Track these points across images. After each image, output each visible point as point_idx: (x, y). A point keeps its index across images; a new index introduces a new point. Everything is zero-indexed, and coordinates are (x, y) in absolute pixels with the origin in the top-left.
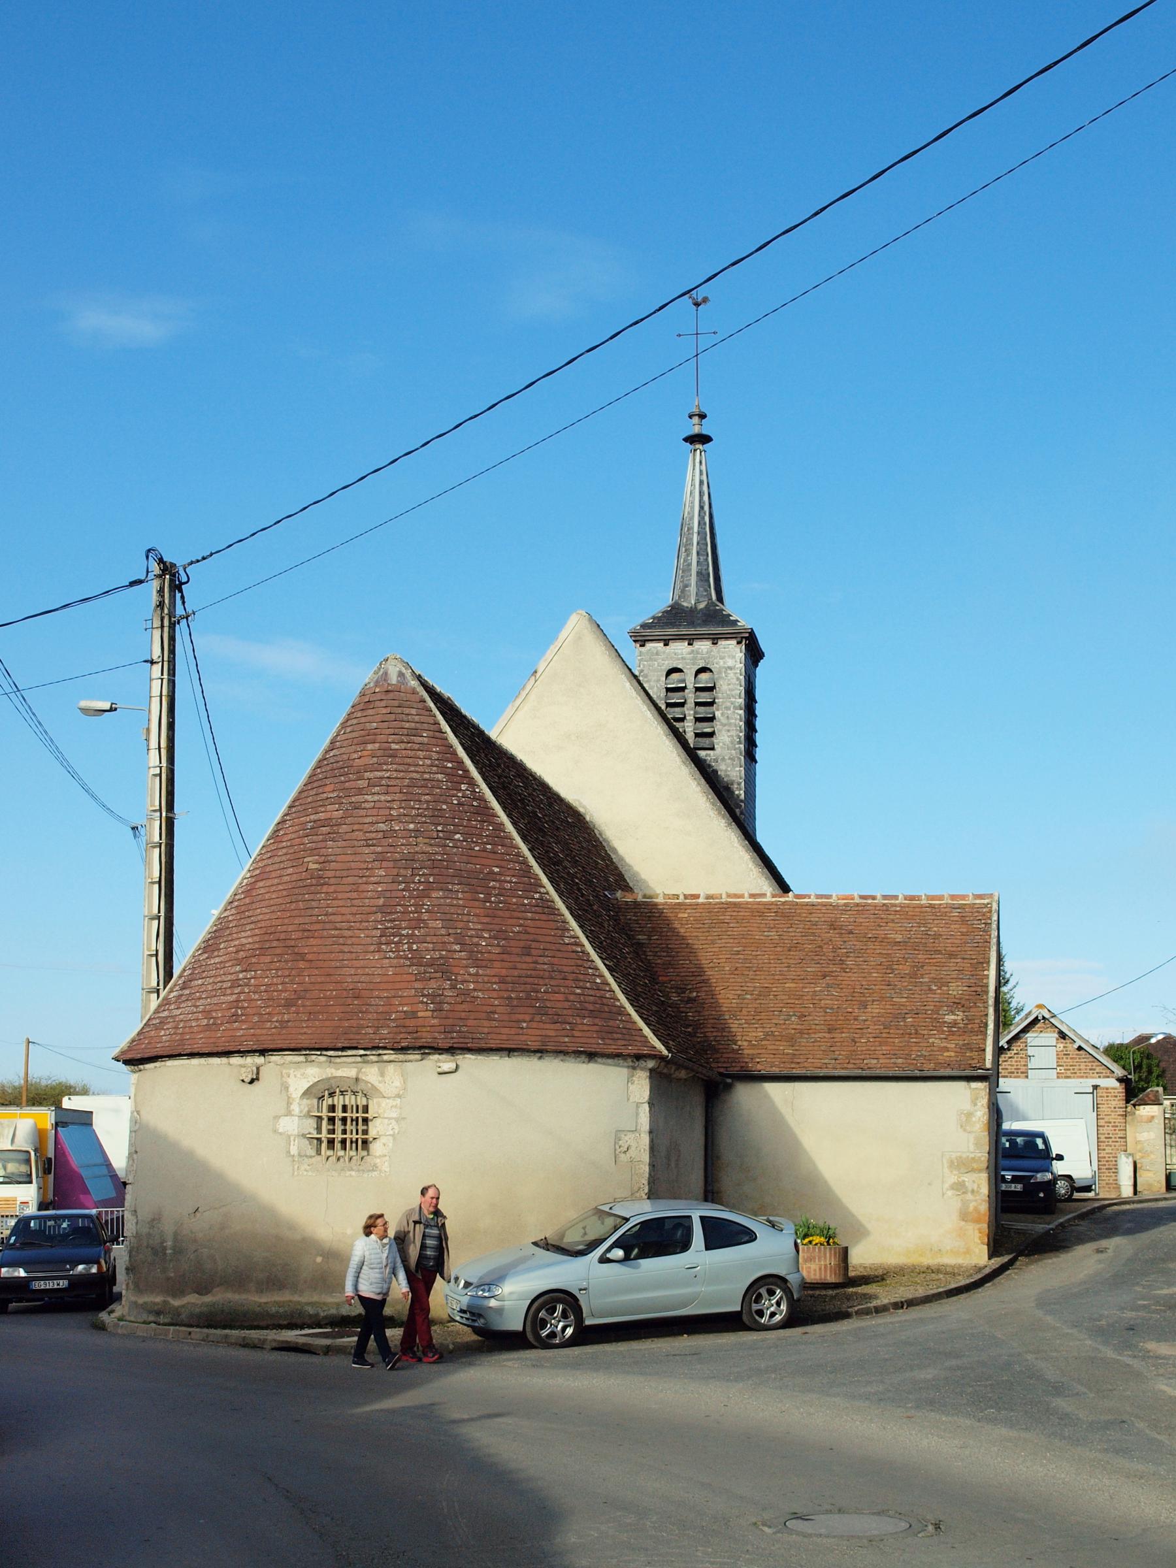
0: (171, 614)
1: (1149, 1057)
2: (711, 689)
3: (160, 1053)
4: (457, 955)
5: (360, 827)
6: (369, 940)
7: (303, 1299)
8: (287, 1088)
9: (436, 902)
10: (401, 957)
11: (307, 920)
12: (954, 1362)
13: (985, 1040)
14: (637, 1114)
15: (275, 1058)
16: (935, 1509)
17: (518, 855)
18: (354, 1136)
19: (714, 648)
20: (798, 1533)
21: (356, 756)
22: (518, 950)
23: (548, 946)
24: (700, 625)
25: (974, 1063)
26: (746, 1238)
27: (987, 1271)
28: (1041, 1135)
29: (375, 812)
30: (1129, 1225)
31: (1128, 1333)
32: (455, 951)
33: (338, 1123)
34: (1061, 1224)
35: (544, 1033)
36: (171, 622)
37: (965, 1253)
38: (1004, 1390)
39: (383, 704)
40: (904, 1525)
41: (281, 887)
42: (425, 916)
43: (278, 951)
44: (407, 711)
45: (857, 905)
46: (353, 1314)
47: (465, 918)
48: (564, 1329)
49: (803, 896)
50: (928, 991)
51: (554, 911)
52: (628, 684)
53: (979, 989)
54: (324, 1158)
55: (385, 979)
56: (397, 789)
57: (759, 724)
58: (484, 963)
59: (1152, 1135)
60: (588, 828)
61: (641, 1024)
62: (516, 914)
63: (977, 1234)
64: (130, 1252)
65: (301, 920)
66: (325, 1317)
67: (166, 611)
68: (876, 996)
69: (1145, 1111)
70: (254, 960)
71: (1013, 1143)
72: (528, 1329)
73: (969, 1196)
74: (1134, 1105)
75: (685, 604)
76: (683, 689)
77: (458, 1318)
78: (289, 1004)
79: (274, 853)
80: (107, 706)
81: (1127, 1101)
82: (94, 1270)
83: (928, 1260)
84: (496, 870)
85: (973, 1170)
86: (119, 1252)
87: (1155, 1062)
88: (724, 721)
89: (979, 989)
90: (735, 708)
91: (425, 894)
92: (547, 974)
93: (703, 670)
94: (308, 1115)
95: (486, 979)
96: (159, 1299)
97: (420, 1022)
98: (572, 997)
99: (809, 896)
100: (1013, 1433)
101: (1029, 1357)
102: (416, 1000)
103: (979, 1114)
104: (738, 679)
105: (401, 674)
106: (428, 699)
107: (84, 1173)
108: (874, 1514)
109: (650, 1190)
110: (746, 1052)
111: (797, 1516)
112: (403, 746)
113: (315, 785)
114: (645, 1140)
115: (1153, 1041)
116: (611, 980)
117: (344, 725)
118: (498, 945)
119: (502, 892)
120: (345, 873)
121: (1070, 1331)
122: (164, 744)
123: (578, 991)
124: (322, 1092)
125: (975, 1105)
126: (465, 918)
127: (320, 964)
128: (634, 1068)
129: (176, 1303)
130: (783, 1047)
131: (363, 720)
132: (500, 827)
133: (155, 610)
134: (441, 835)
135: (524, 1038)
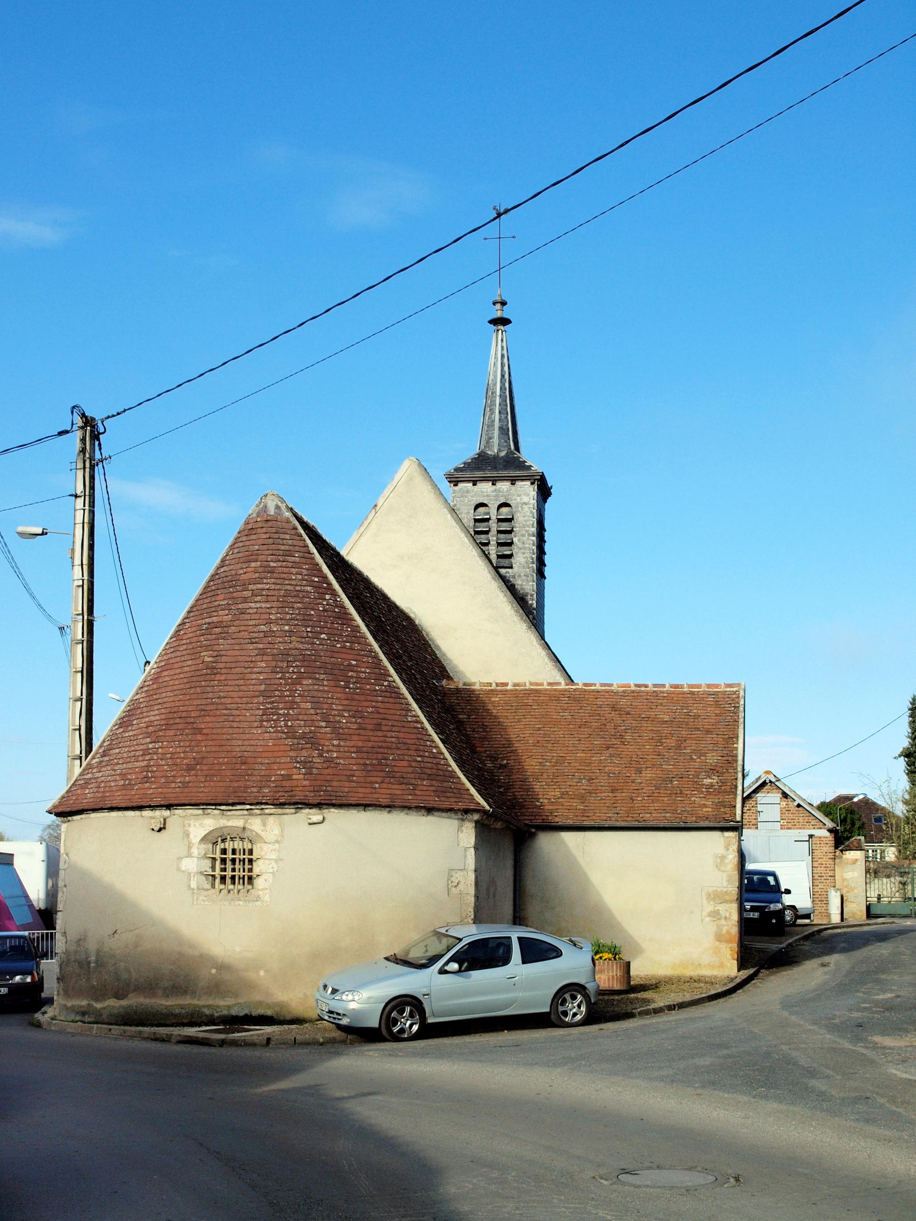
0: (92, 458)
1: (852, 812)
2: (510, 520)
3: (86, 807)
4: (323, 730)
5: (246, 628)
6: (253, 718)
7: (201, 1003)
8: (188, 835)
9: (306, 688)
10: (279, 732)
11: (204, 702)
12: (725, 1052)
13: (735, 798)
14: (465, 857)
15: (179, 812)
16: (741, 1168)
17: (371, 651)
18: (242, 874)
19: (513, 487)
20: (631, 1185)
21: (242, 572)
22: (370, 727)
23: (395, 723)
24: (501, 470)
25: (727, 816)
26: (555, 954)
27: (738, 980)
28: (773, 874)
29: (257, 616)
30: (842, 945)
31: (858, 1029)
32: (322, 727)
33: (229, 863)
34: (790, 944)
35: (392, 792)
36: (91, 463)
37: (719, 967)
38: (766, 1073)
39: (264, 530)
40: (712, 1178)
41: (182, 676)
42: (298, 700)
43: (180, 727)
44: (282, 536)
45: (633, 692)
46: (241, 1014)
47: (330, 701)
48: (411, 1026)
49: (591, 685)
50: (680, 758)
51: (399, 696)
52: (449, 516)
53: (730, 758)
54: (218, 891)
55: (266, 749)
56: (275, 599)
57: (547, 548)
58: (344, 737)
59: (856, 874)
60: (418, 630)
61: (468, 785)
62: (369, 698)
63: (729, 952)
64: (61, 966)
65: (199, 702)
66: (219, 1017)
67: (87, 455)
68: (649, 764)
69: (851, 855)
70: (161, 734)
71: (751, 880)
72: (383, 1026)
73: (723, 922)
74: (842, 851)
75: (489, 453)
76: (488, 520)
77: (326, 1018)
78: (189, 768)
79: (177, 648)
80: (40, 531)
81: (836, 847)
82: (29, 980)
83: (689, 972)
84: (354, 663)
85: (726, 901)
86: (49, 967)
87: (856, 817)
88: (520, 545)
89: (730, 758)
90: (529, 535)
91: (298, 682)
92: (394, 745)
93: (478, 506)
94: (205, 857)
95: (346, 749)
96: (84, 1003)
97: (294, 783)
98: (414, 764)
99: (595, 685)
100: (783, 1107)
101: (784, 1047)
102: (290, 766)
103: (731, 857)
104: (531, 512)
105: (277, 507)
106: (299, 527)
107: (9, 903)
108: (685, 1169)
109: (475, 916)
110: (546, 807)
111: (626, 1172)
112: (280, 564)
113: (210, 594)
114: (472, 877)
115: (855, 800)
116: (444, 750)
117: (232, 547)
118: (356, 723)
119: (359, 680)
120: (233, 665)
121: (812, 1028)
122: (85, 562)
123: (419, 759)
124: (216, 838)
125: (728, 850)
126: (330, 701)
127: (215, 737)
128: (463, 820)
129: (98, 1006)
130: (575, 803)
131: (248, 543)
132: (356, 629)
133: (79, 455)
134: (310, 634)
135: (376, 796)
